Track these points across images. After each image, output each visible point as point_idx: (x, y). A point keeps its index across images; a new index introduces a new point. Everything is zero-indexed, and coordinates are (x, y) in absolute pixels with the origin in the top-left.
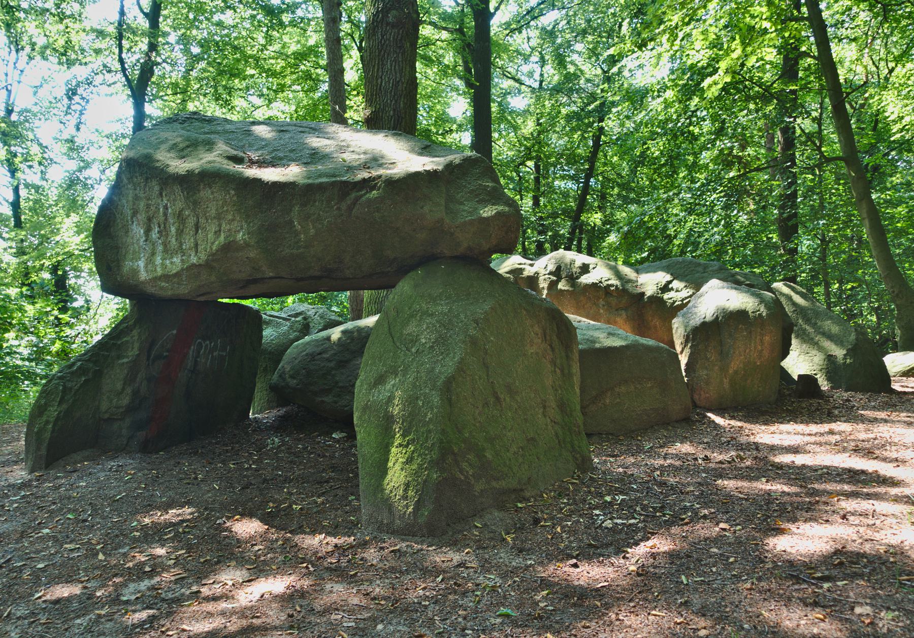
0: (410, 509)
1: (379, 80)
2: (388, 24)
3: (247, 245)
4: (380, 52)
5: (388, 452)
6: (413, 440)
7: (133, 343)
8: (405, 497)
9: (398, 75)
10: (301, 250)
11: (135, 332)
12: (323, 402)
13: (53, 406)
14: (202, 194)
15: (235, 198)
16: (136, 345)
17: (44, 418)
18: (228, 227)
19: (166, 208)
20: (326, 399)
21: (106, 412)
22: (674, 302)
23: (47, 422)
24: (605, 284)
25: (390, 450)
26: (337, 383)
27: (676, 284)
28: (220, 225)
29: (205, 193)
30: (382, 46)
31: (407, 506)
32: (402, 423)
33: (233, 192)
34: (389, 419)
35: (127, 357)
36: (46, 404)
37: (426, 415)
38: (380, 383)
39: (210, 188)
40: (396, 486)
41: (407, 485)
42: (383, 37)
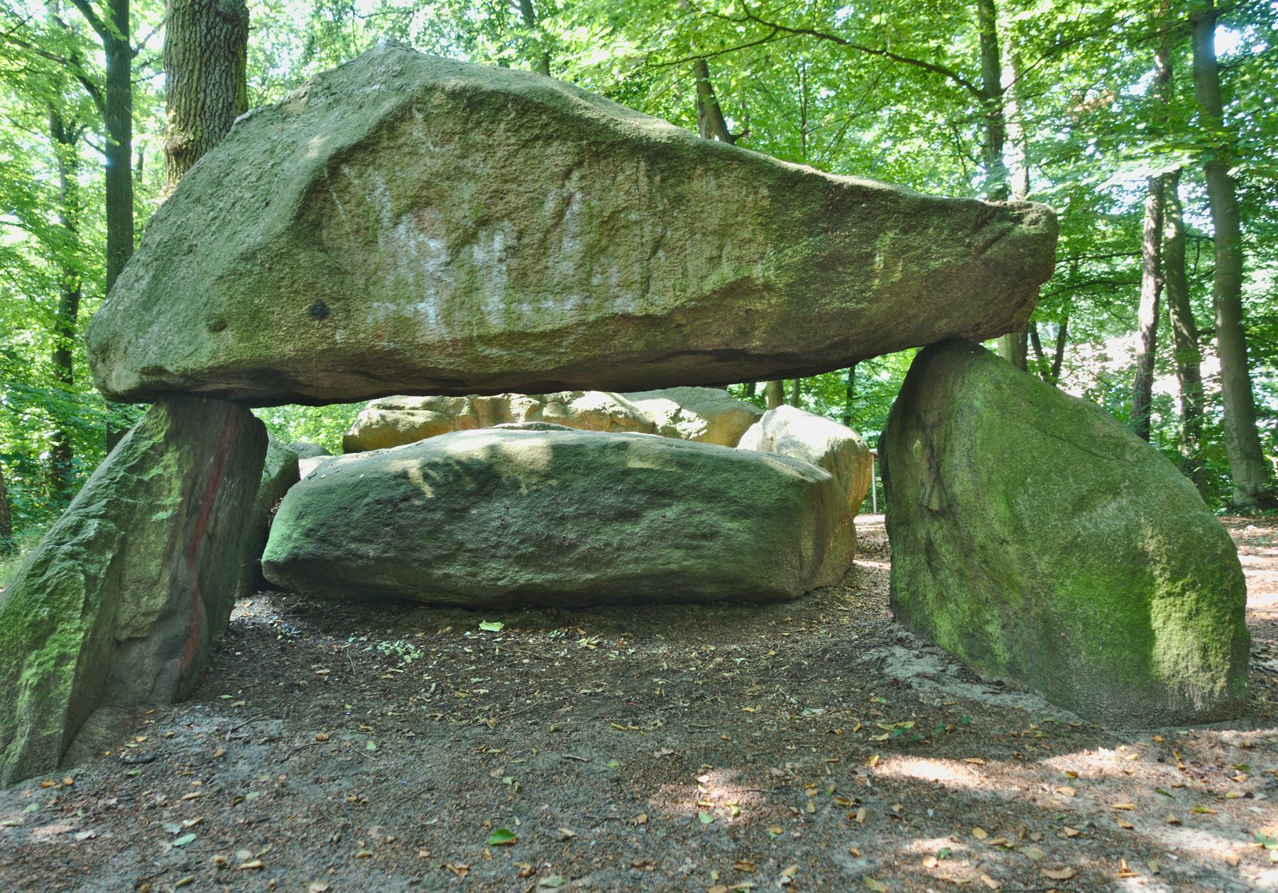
0: (1222, 682)
1: (201, 96)
2: (218, 13)
3: (768, 287)
4: (203, 54)
5: (1147, 606)
6: (1194, 584)
7: (169, 480)
8: (1206, 668)
9: (231, 94)
10: (864, 305)
11: (170, 458)
12: (447, 576)
13: (70, 620)
14: (696, 185)
15: (766, 203)
16: (177, 484)
17: (52, 649)
18: (736, 252)
19: (568, 201)
20: (451, 571)
21: (127, 625)
22: (690, 434)
23: (62, 659)
24: (610, 411)
25: (1150, 604)
26: (461, 544)
27: (685, 413)
28: (721, 248)
29: (703, 185)
30: (208, 44)
31: (1214, 680)
32: (1168, 562)
33: (765, 192)
34: (1139, 559)
35: (164, 508)
36: (52, 617)
37: (1214, 546)
38: (1082, 509)
39: (717, 177)
40: (1183, 653)
41: (1205, 650)
42: (209, 30)
